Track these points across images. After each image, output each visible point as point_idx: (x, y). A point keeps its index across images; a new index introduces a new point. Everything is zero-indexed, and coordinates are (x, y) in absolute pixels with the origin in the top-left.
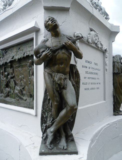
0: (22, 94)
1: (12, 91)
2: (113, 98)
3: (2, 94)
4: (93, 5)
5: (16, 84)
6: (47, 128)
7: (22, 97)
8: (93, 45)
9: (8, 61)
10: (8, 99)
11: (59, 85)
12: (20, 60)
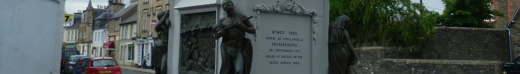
1: (195, 63)
3: (185, 68)
5: (199, 55)
7: (205, 69)
8: (285, 12)
9: (192, 30)
11: (231, 56)
12: (204, 30)
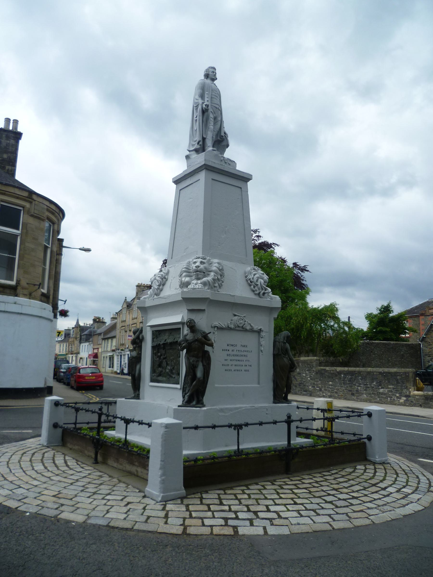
0: (172, 373)
1: (164, 371)
2: (272, 383)
3: (155, 374)
4: (247, 281)
5: (167, 364)
6: (185, 394)
8: (237, 329)
9: (161, 343)
10: (160, 378)
11: (193, 365)
12: (171, 344)
